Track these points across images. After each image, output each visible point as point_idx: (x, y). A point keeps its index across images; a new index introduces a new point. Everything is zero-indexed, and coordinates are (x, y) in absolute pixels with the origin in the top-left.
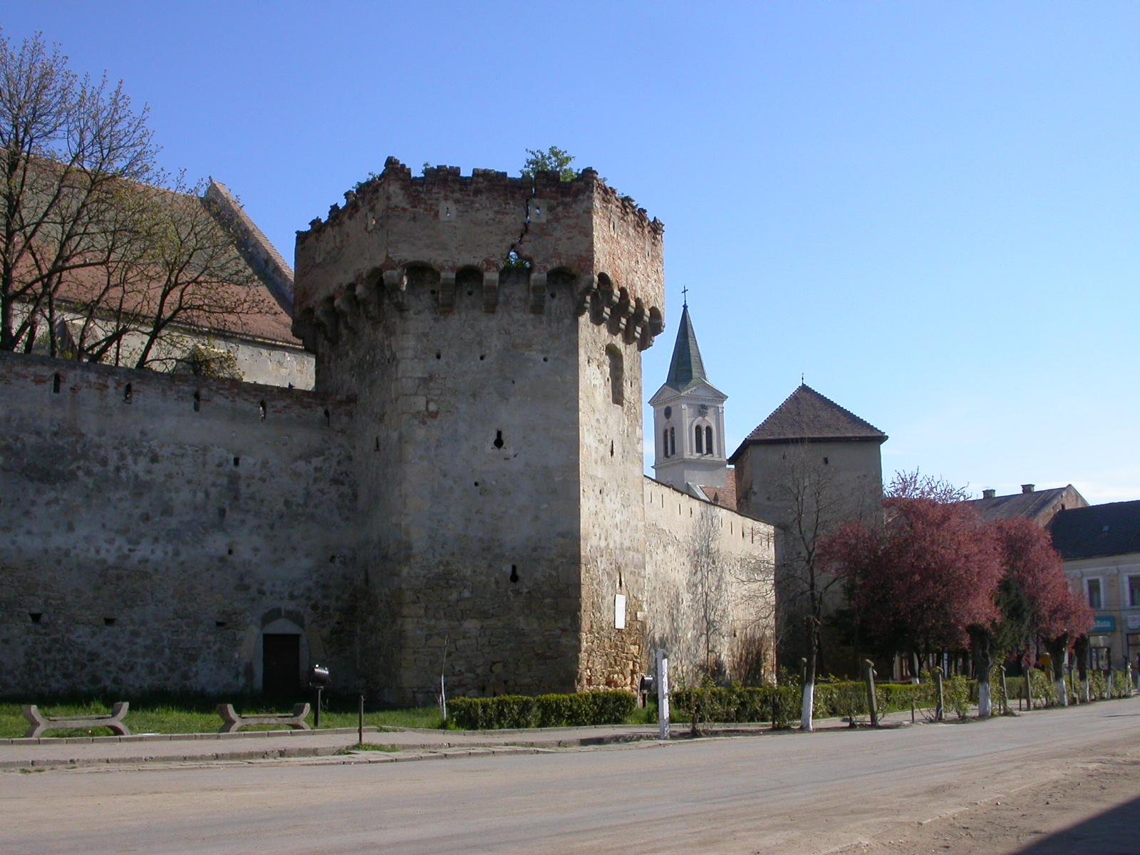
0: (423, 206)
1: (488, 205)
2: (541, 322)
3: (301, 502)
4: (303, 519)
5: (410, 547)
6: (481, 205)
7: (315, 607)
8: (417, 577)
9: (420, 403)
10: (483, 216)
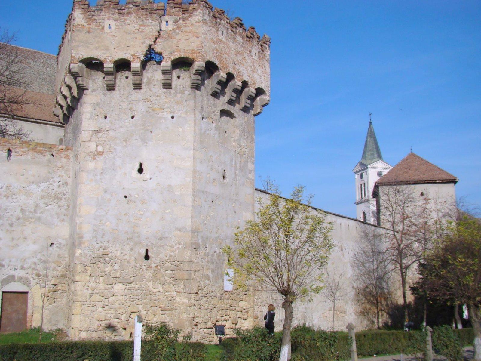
0: (94, 23)
1: (135, 21)
2: (170, 94)
3: (32, 210)
4: (33, 220)
5: (81, 238)
6: (131, 21)
7: (38, 275)
8: (86, 256)
9: (92, 146)
10: (131, 28)
